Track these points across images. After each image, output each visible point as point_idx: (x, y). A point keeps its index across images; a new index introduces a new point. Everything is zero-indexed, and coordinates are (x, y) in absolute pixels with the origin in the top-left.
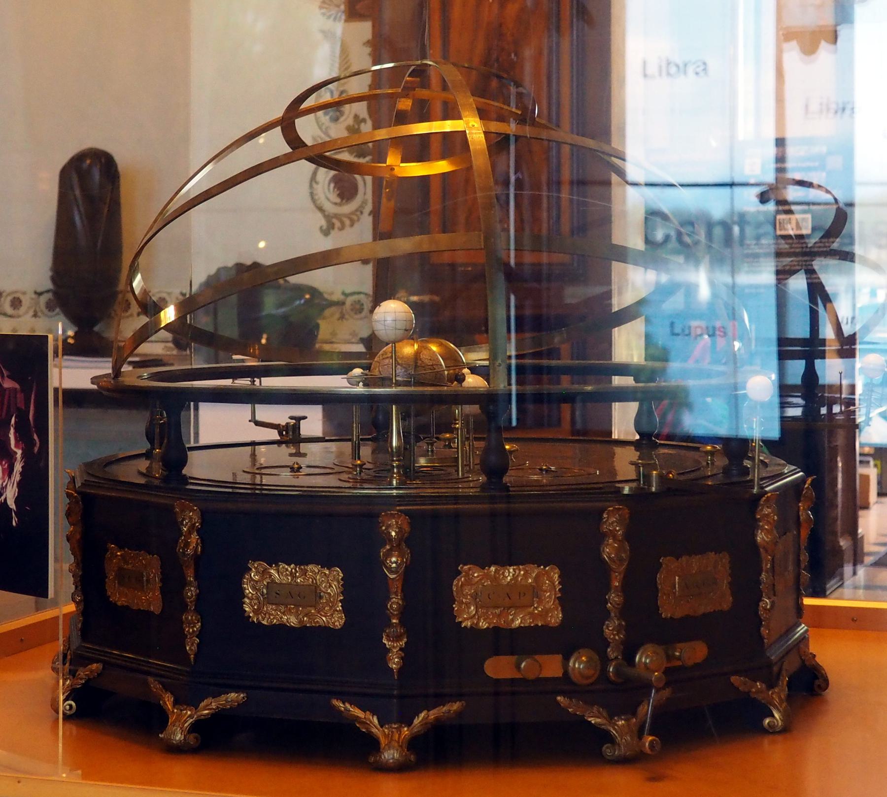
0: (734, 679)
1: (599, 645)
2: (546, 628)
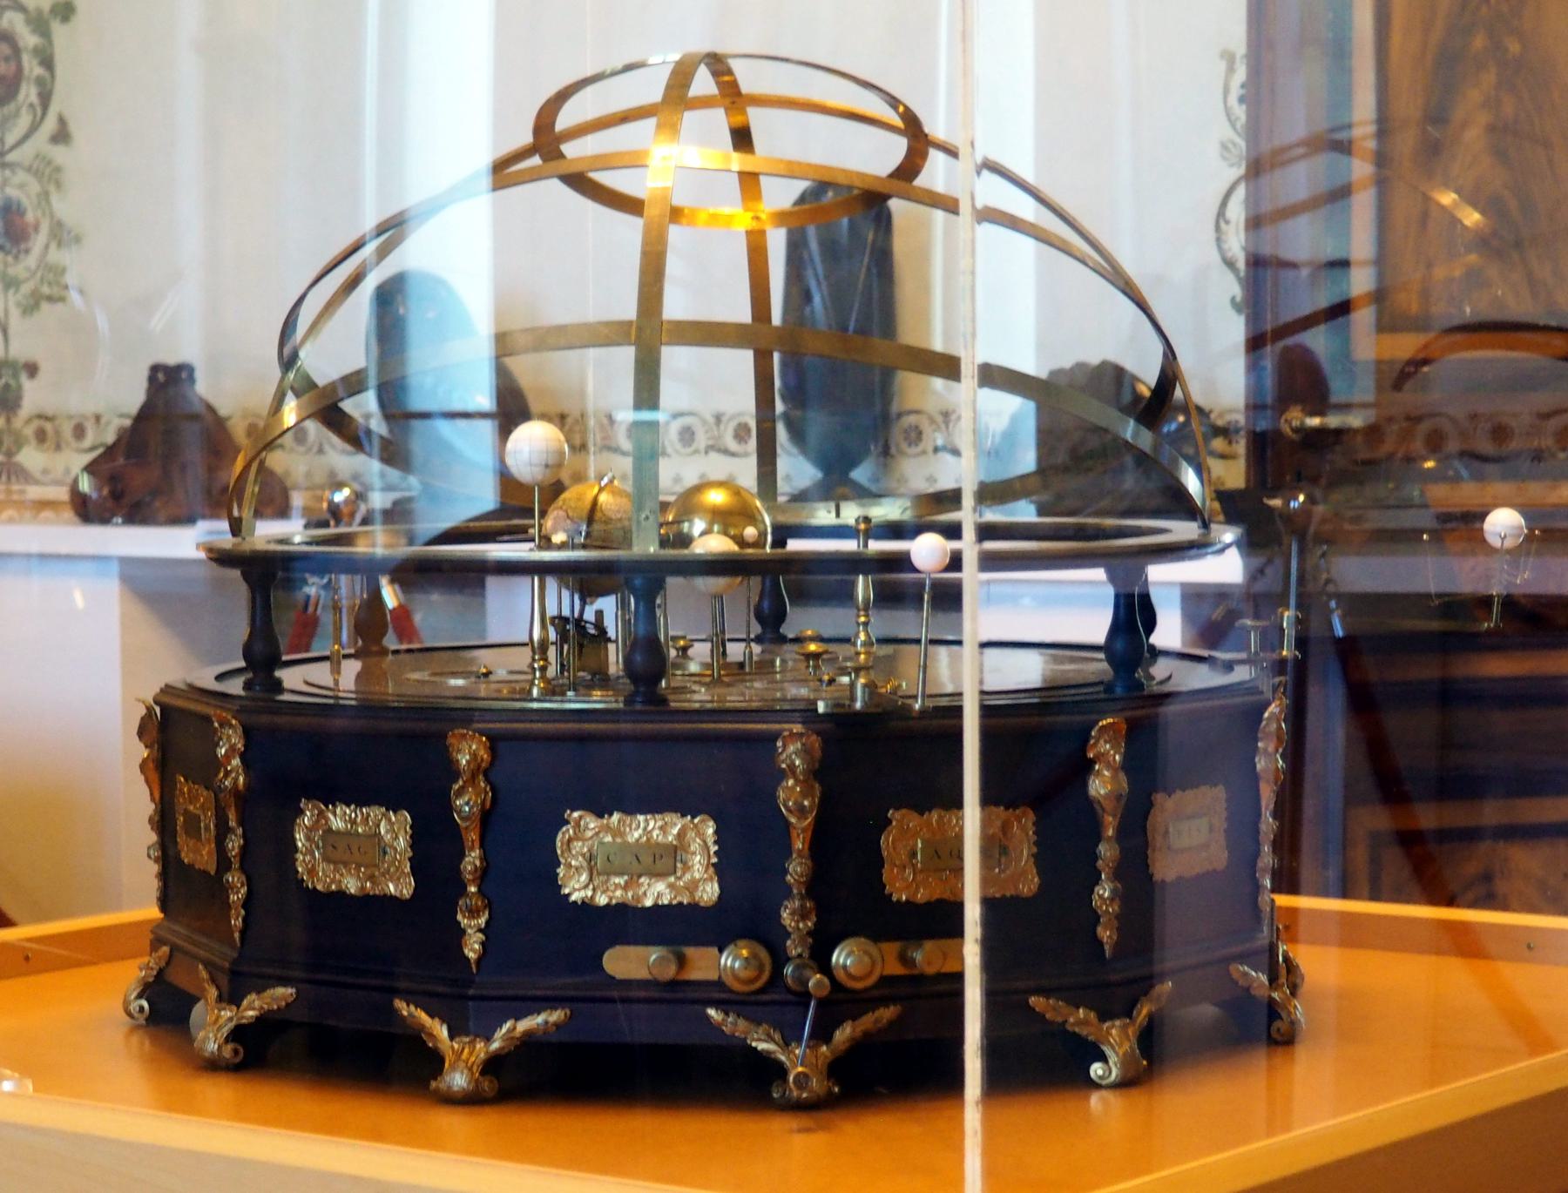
0: (1033, 1000)
1: (770, 939)
2: (694, 907)
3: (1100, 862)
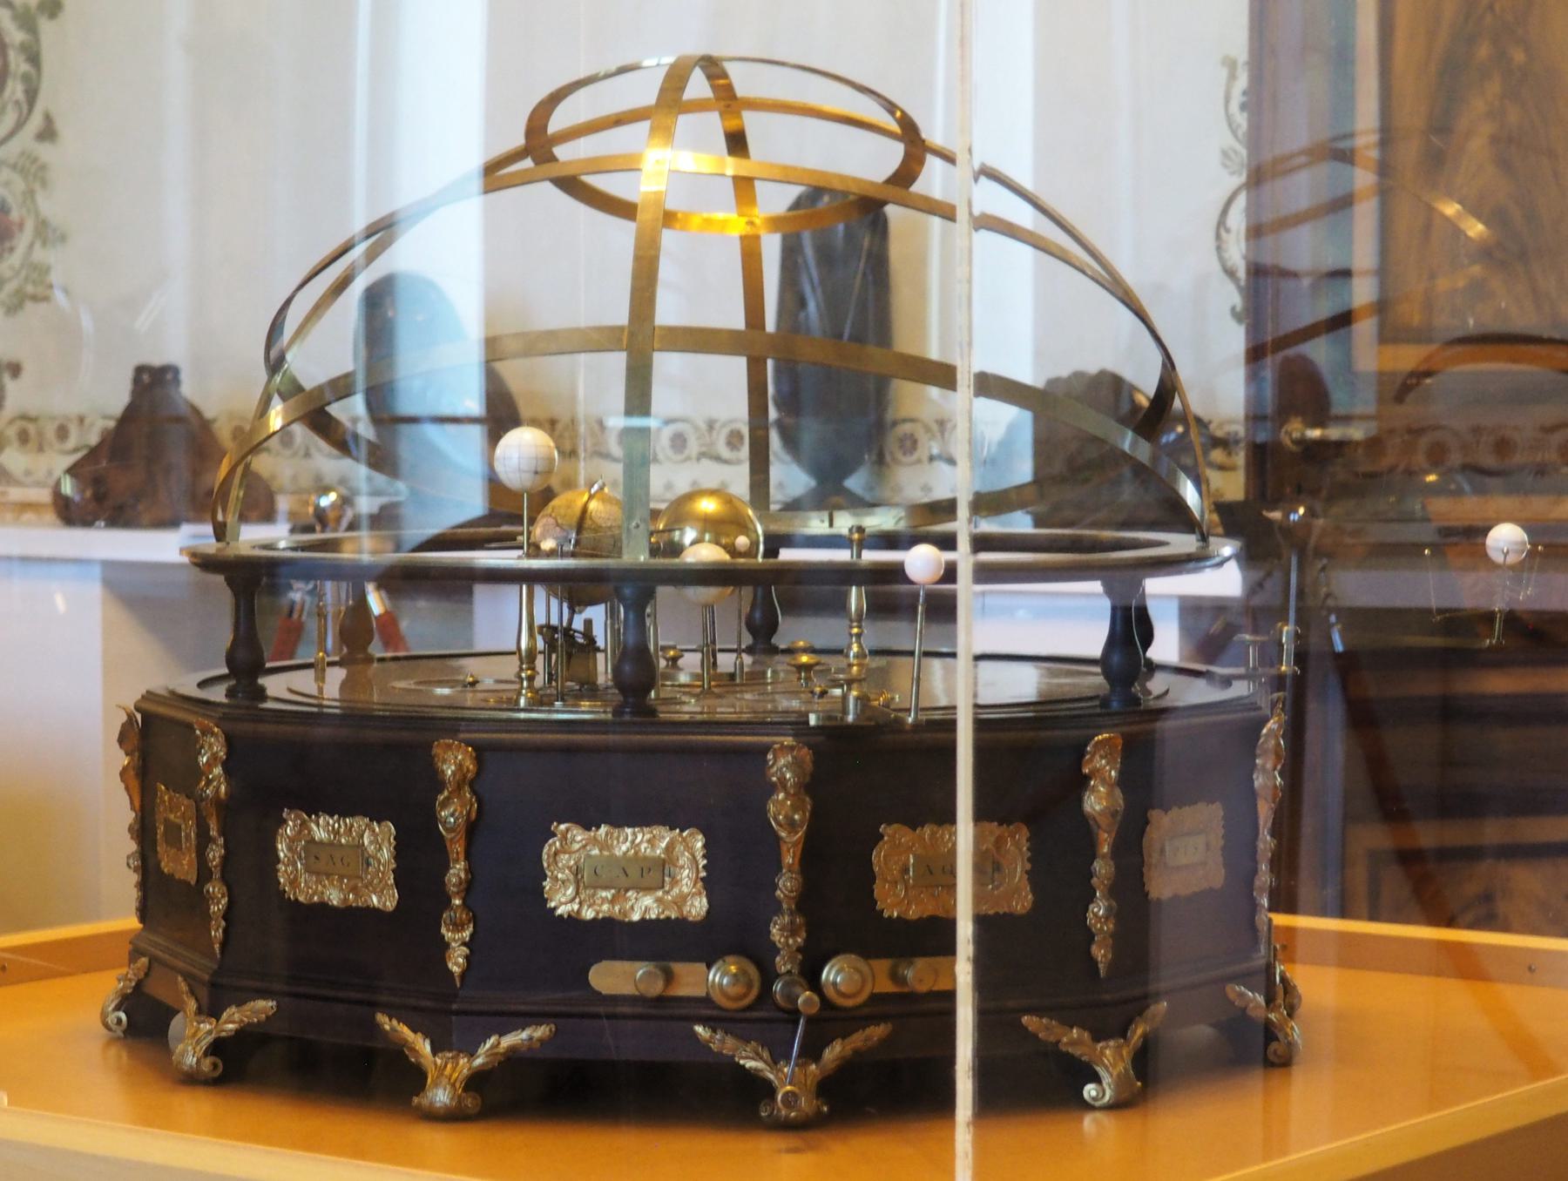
1: (760, 955)
2: (682, 922)
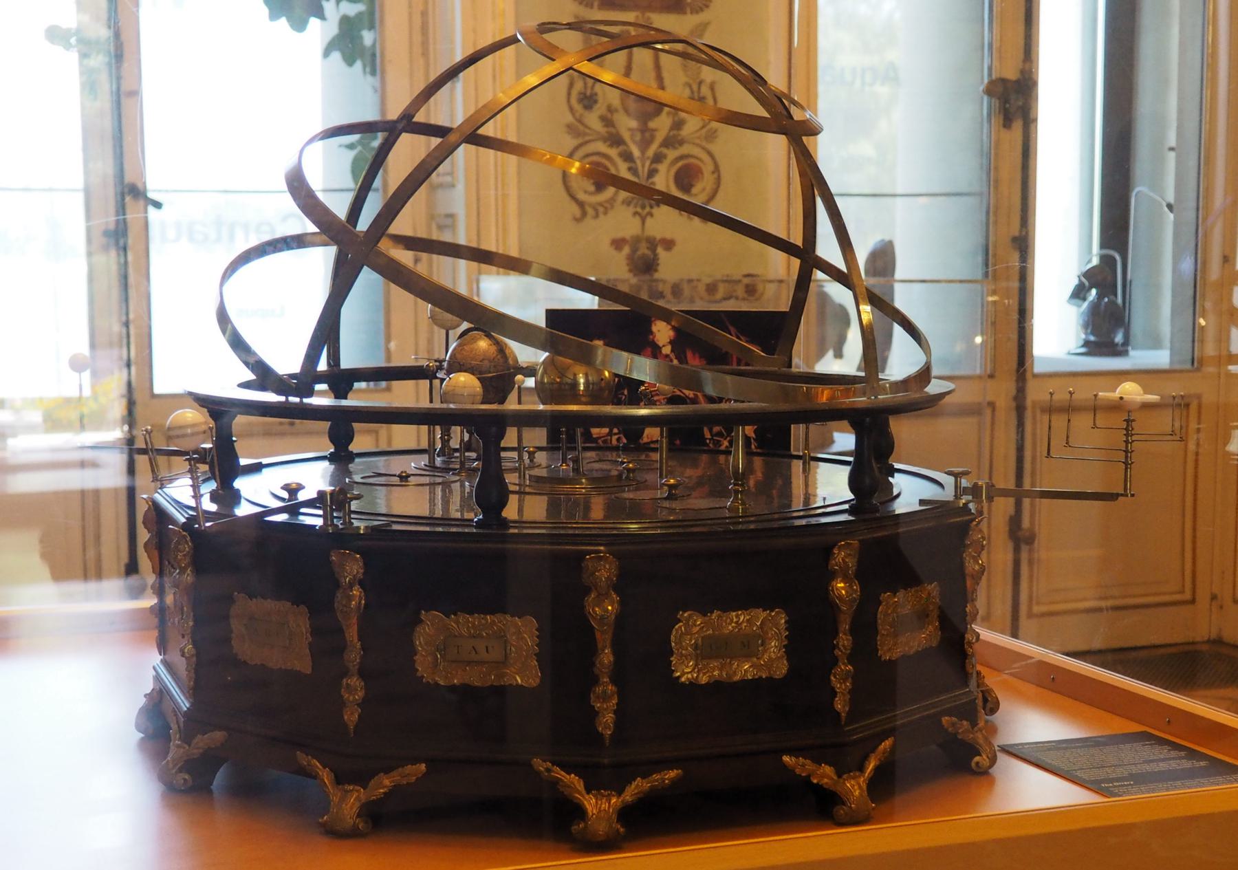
3: (837, 652)
